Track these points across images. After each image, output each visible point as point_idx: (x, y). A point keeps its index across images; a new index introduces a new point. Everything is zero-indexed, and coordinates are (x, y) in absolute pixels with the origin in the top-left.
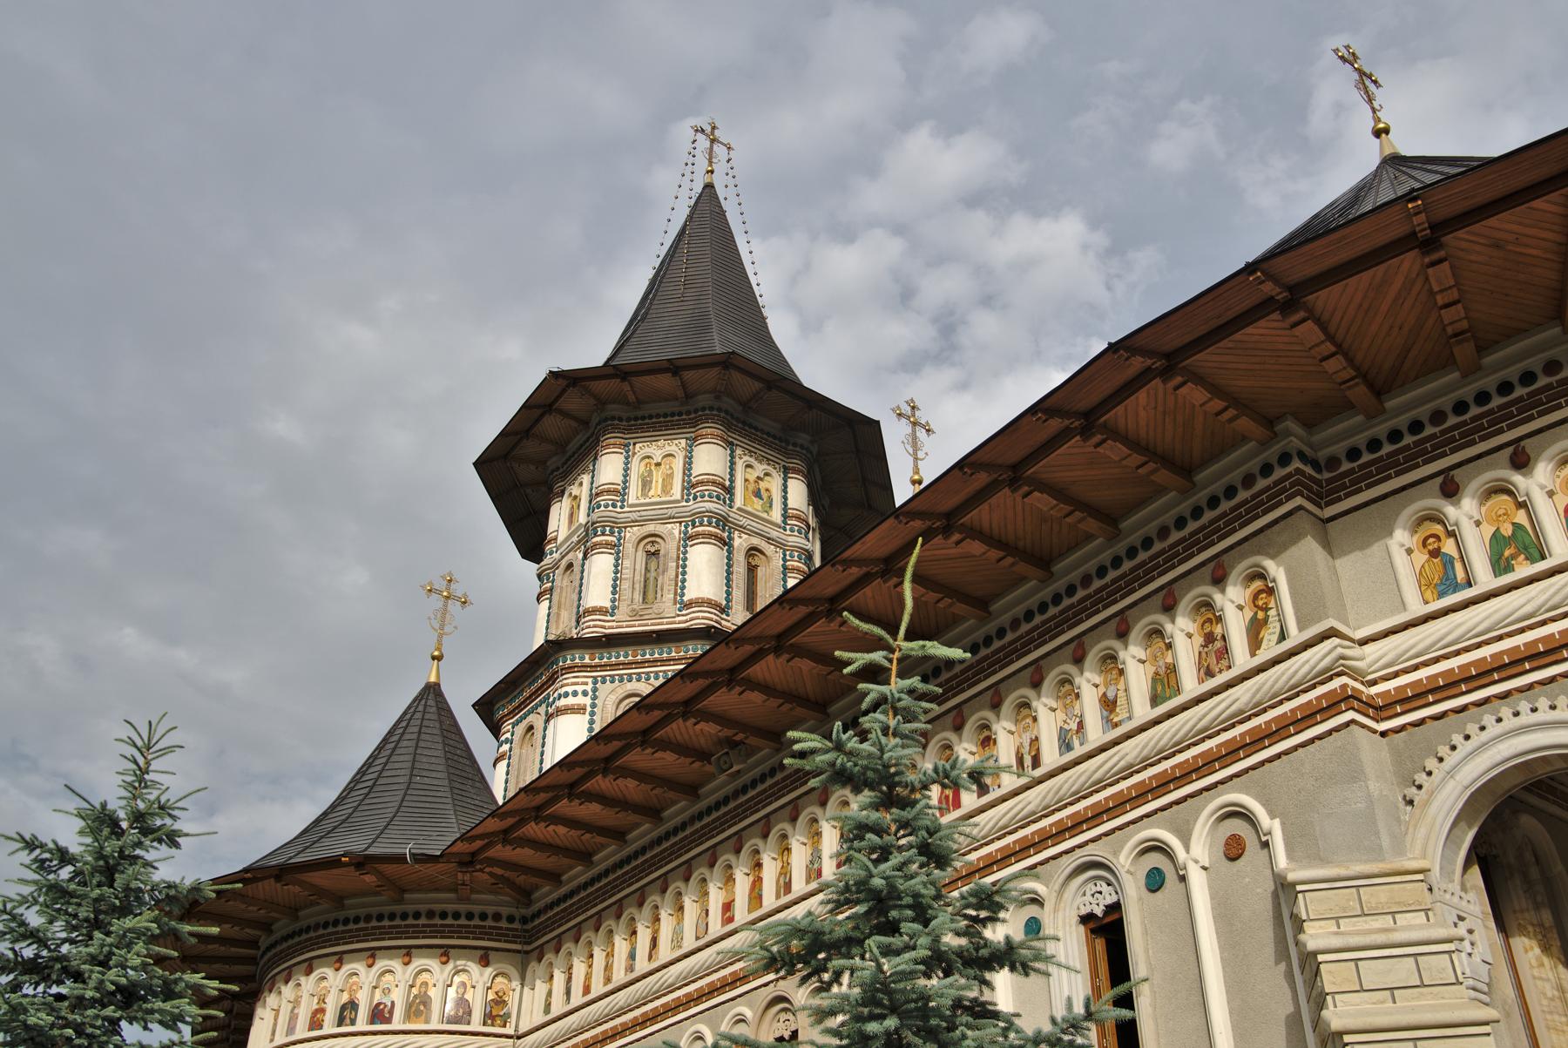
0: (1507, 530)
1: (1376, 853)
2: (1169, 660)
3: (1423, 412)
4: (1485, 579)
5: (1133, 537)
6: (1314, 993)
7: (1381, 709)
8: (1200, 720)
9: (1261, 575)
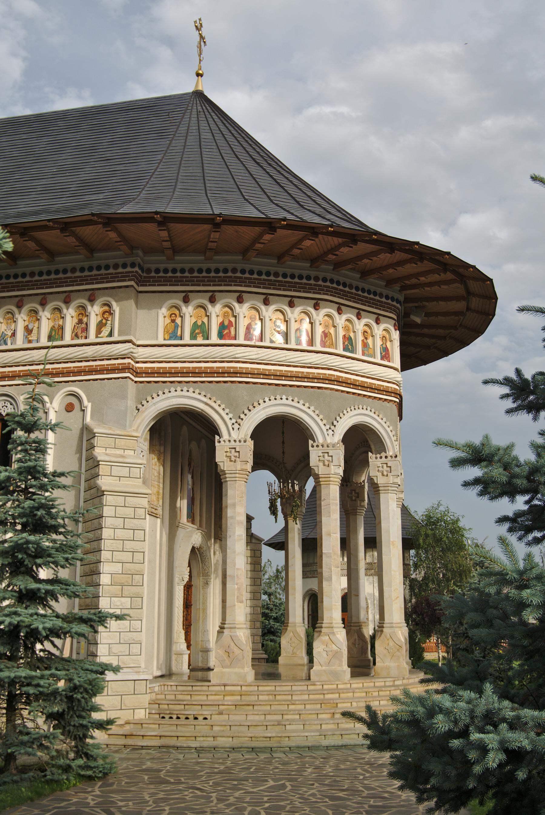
0: (199, 323)
1: (124, 427)
2: (61, 323)
3: (187, 266)
4: (187, 340)
5: (60, 265)
6: (93, 471)
7: (138, 373)
8: (69, 355)
9: (109, 305)
